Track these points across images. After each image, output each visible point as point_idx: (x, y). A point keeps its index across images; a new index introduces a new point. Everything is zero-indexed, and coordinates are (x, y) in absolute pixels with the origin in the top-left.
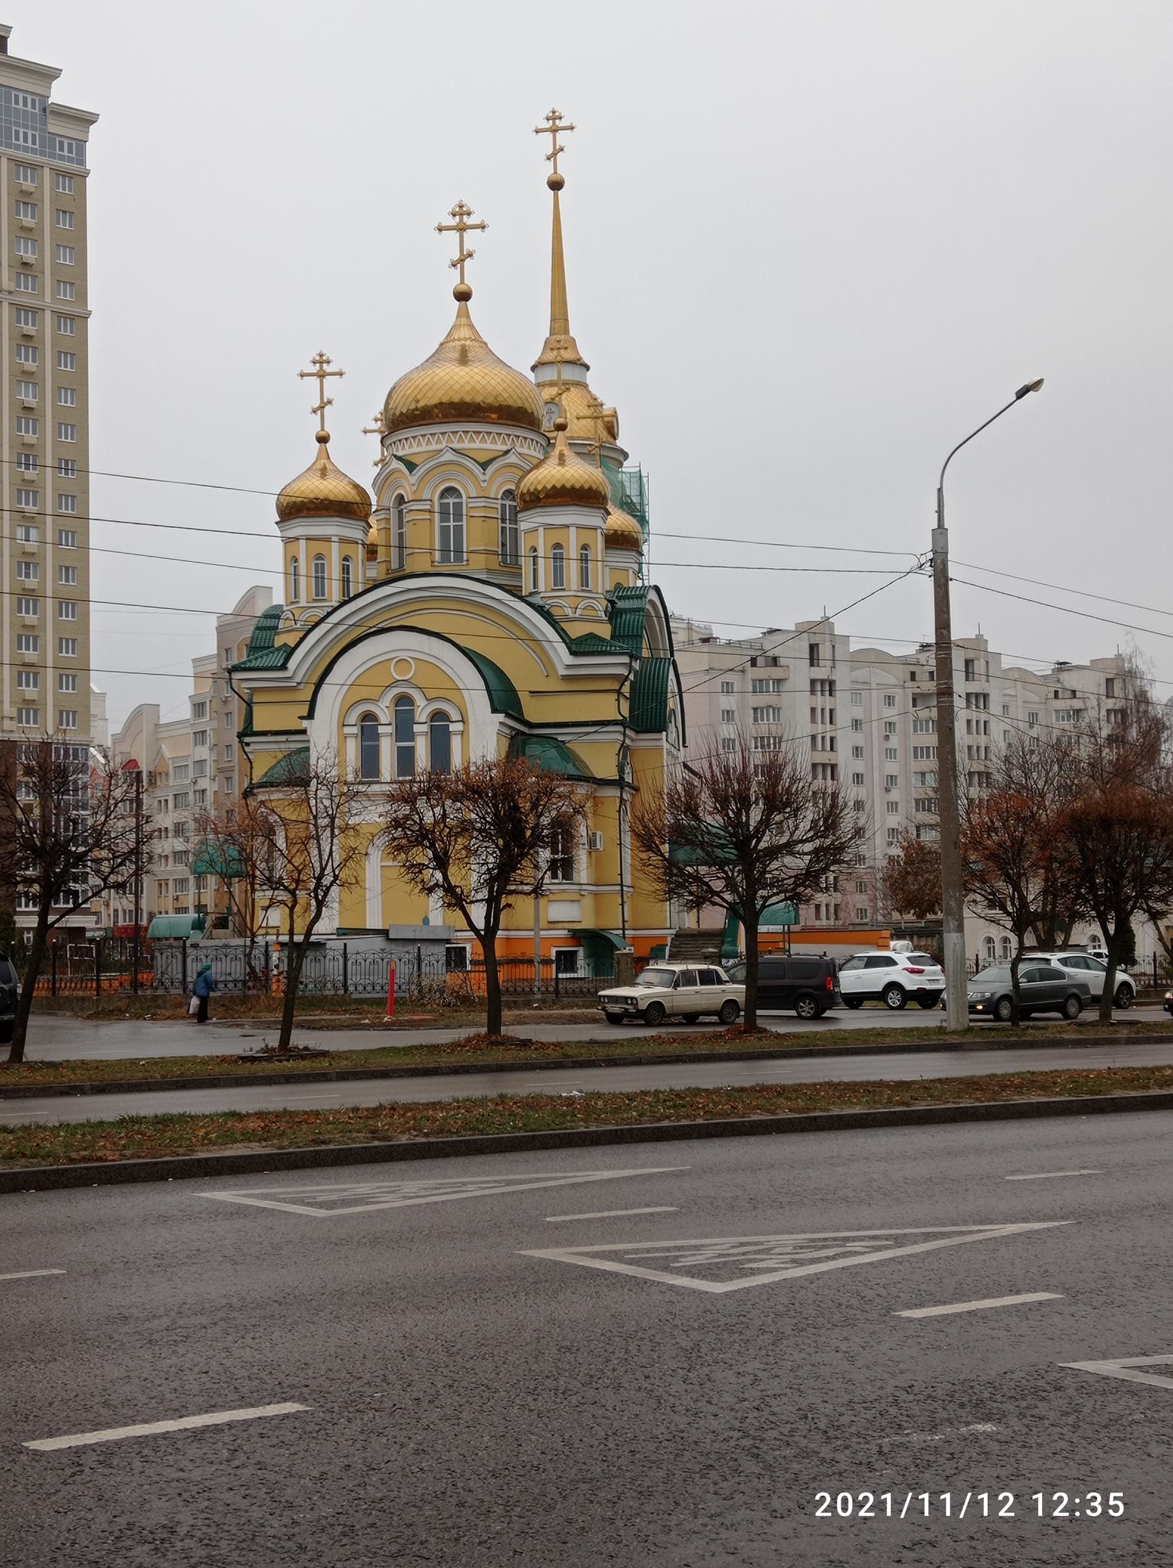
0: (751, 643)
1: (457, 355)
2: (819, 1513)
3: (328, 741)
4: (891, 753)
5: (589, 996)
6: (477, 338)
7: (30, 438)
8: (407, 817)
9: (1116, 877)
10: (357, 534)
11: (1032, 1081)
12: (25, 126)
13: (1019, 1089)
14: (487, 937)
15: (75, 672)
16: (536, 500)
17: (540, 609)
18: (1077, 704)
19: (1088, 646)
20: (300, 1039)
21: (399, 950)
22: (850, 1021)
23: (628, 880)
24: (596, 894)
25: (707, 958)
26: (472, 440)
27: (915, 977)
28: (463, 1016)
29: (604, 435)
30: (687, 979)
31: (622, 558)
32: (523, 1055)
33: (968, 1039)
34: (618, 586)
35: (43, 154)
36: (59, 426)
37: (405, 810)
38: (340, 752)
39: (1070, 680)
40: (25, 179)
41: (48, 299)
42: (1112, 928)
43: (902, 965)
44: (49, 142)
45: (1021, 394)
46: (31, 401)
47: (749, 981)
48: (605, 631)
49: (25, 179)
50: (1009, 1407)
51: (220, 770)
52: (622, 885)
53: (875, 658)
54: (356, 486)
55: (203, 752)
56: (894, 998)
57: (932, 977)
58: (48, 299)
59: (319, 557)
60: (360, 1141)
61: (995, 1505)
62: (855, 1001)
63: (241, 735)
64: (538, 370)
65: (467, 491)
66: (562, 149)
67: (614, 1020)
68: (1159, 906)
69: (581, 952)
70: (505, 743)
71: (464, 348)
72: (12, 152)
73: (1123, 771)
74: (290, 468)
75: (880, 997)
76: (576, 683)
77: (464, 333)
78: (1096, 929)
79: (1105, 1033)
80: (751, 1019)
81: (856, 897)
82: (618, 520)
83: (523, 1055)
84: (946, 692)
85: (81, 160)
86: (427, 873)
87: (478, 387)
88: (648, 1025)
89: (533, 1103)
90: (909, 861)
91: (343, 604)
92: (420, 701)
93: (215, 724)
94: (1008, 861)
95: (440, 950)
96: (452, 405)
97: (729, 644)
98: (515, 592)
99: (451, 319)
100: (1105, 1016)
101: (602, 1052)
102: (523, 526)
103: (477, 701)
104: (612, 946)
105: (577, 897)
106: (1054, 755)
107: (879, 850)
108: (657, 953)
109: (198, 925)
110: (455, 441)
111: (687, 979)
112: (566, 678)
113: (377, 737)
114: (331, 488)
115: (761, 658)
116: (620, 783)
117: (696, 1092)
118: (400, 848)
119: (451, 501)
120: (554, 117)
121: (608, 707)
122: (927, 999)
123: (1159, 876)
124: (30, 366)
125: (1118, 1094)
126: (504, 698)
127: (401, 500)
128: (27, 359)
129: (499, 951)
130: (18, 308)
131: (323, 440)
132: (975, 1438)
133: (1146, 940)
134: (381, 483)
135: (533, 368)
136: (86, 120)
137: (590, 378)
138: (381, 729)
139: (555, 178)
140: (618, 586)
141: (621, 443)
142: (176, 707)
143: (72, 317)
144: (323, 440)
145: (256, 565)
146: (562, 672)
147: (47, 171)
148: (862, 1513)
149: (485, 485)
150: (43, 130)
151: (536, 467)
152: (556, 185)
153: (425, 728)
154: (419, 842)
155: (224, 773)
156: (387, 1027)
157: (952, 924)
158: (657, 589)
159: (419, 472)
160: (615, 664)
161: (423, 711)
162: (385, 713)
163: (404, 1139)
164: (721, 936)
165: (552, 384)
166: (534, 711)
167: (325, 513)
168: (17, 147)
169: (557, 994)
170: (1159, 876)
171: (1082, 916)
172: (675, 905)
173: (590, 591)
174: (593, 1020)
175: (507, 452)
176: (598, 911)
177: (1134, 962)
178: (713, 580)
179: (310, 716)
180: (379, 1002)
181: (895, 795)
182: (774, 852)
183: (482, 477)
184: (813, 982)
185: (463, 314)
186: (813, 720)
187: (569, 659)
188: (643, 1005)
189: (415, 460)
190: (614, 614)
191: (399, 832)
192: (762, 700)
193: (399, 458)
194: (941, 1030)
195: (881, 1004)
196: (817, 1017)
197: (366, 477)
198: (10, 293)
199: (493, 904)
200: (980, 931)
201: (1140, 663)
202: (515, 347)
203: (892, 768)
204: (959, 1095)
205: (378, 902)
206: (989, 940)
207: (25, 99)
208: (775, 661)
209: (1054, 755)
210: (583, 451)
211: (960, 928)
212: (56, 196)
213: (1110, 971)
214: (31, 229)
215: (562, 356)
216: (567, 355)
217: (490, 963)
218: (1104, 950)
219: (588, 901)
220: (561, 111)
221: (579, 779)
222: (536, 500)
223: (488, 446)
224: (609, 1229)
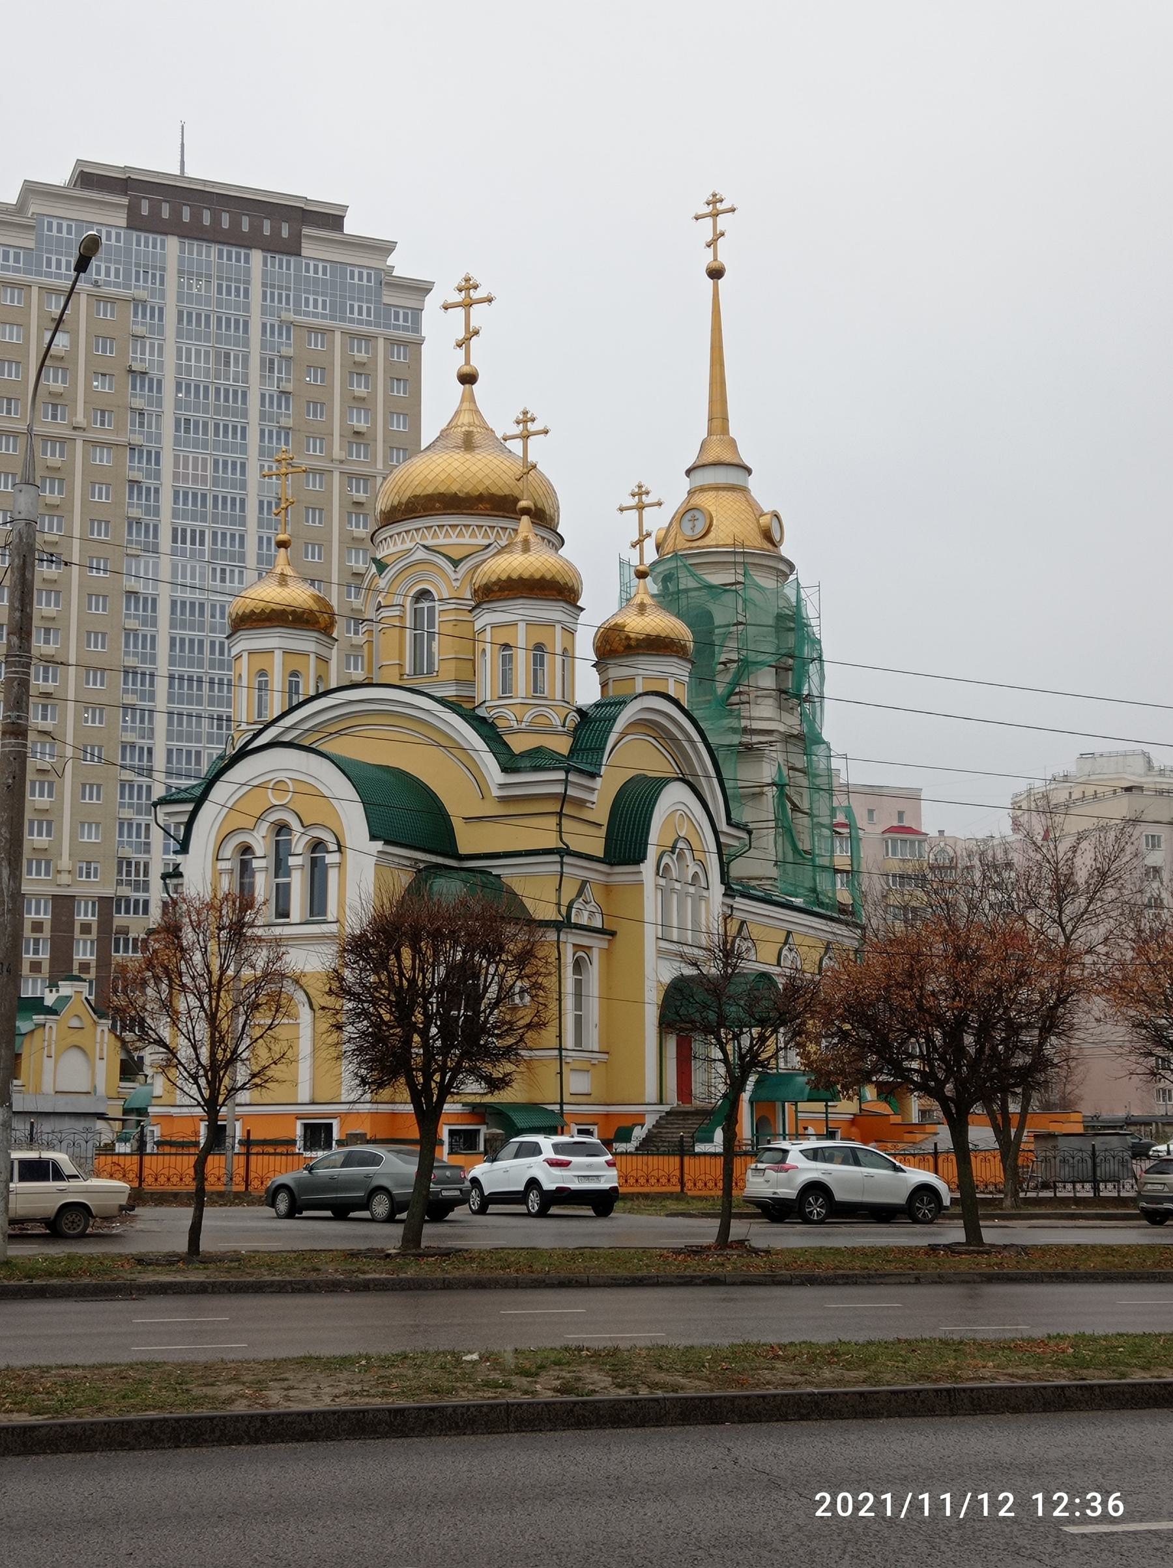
1: (460, 442)
2: (819, 1513)
12: (316, 293)
26: (447, 535)
27: (556, 1171)
35: (377, 325)
40: (359, 351)
41: (380, 466)
44: (384, 313)
49: (359, 351)
52: (560, 1049)
58: (380, 466)
59: (294, 674)
61: (995, 1505)
64: (692, 474)
65: (439, 592)
66: (722, 234)
72: (346, 325)
87: (455, 474)
105: (586, 1066)
110: (429, 538)
112: (503, 800)
119: (425, 605)
120: (715, 200)
128: (357, 526)
130: (350, 476)
137: (752, 482)
139: (715, 265)
141: (785, 551)
146: (496, 792)
147: (381, 342)
148: (862, 1513)
149: (457, 584)
150: (378, 302)
152: (716, 273)
159: (390, 573)
161: (299, 843)
162: (260, 841)
167: (268, 624)
168: (352, 321)
173: (545, 698)
175: (490, 545)
183: (453, 576)
185: (470, 398)
187: (501, 778)
189: (388, 561)
198: (341, 462)
207: (360, 274)
212: (389, 365)
214: (364, 399)
222: (494, 592)
223: (467, 540)
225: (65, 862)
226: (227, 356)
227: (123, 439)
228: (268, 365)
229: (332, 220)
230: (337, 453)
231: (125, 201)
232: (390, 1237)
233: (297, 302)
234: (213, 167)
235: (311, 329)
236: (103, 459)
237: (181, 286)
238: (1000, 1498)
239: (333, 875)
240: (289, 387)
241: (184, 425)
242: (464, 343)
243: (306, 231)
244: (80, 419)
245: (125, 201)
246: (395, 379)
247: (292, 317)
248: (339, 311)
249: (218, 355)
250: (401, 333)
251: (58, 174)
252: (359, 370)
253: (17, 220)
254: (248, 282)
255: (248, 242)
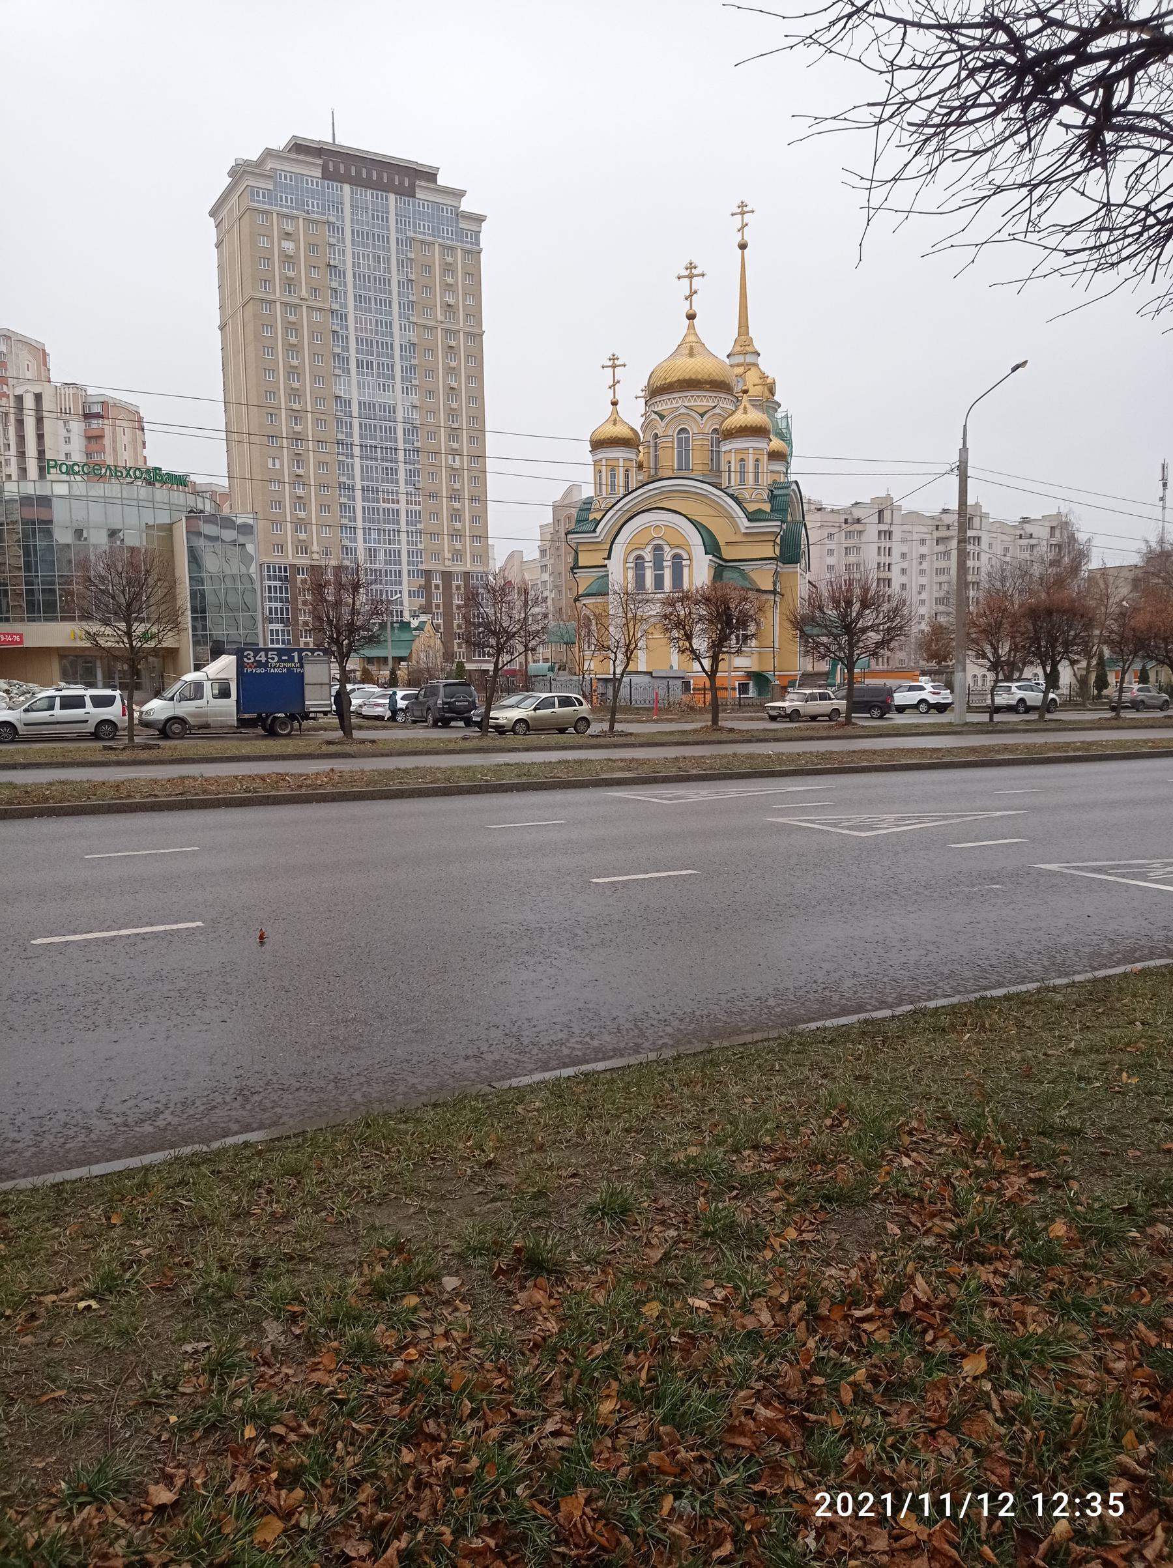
0: (845, 511)
3: (618, 572)
4: (922, 572)
5: (762, 707)
6: (699, 341)
7: (454, 405)
8: (671, 614)
9: (1053, 643)
10: (633, 456)
11: (1005, 748)
13: (998, 752)
14: (712, 675)
15: (481, 537)
16: (730, 434)
17: (731, 496)
18: (1033, 542)
19: (1039, 509)
20: (618, 727)
21: (657, 682)
22: (899, 719)
23: (777, 646)
24: (760, 653)
25: (820, 686)
28: (692, 716)
29: (767, 394)
30: (813, 697)
31: (779, 467)
32: (731, 736)
33: (965, 728)
34: (775, 481)
36: (469, 398)
37: (670, 610)
38: (626, 577)
39: (1029, 528)
42: (1048, 669)
43: (929, 690)
44: (460, 234)
45: (1014, 369)
46: (454, 384)
47: (849, 697)
48: (767, 507)
50: (1006, 880)
51: (555, 586)
53: (915, 517)
54: (632, 429)
55: (546, 577)
56: (923, 708)
57: (945, 696)
60: (674, 772)
62: (901, 709)
63: (572, 569)
67: (773, 719)
68: (1076, 657)
69: (751, 683)
70: (713, 571)
71: (691, 347)
73: (1060, 582)
74: (596, 420)
75: (915, 707)
76: (751, 537)
77: (692, 338)
78: (1039, 670)
79: (1042, 726)
80: (848, 718)
81: (902, 655)
82: (776, 444)
83: (731, 736)
84: (963, 541)
85: (478, 244)
86: (681, 642)
88: (791, 721)
89: (751, 756)
90: (934, 633)
91: (625, 496)
92: (667, 548)
93: (552, 561)
94: (991, 633)
95: (679, 682)
96: (685, 380)
97: (832, 511)
98: (717, 486)
99: (685, 331)
100: (1042, 716)
101: (771, 735)
102: (724, 449)
103: (698, 551)
104: (767, 680)
106: (1018, 572)
107: (919, 628)
108: (792, 684)
109: (551, 669)
111: (813, 697)
112: (745, 534)
113: (644, 568)
114: (620, 431)
115: (850, 521)
116: (774, 592)
117: (832, 753)
118: (667, 629)
121: (769, 551)
122: (941, 708)
123: (1078, 641)
124: (453, 364)
125: (1051, 755)
126: (712, 547)
127: (656, 436)
129: (718, 683)
131: (614, 404)
132: (992, 890)
133: (1066, 675)
134: (646, 426)
135: (728, 356)
136: (479, 219)
138: (646, 564)
140: (775, 481)
142: (532, 553)
143: (474, 335)
144: (614, 404)
145: (580, 475)
146: (744, 531)
151: (731, 415)
152: (743, 246)
153: (669, 563)
154: (678, 627)
155: (557, 588)
156: (655, 721)
157: (960, 668)
158: (796, 483)
159: (667, 420)
160: (773, 526)
161: (668, 553)
162: (648, 557)
163: (694, 772)
164: (826, 675)
165: (739, 365)
166: (727, 553)
168: (443, 238)
169: (740, 705)
170: (1078, 641)
171: (1032, 663)
172: (809, 660)
174: (762, 719)
176: (760, 661)
177: (1058, 688)
178: (825, 478)
179: (609, 558)
180: (648, 709)
181: (924, 596)
182: (864, 630)
184: (880, 699)
185: (691, 327)
186: (879, 554)
188: (789, 711)
190: (772, 498)
191: (667, 622)
192: (850, 543)
193: (656, 413)
194: (950, 724)
195: (915, 711)
196: (881, 717)
197: (637, 423)
199: (715, 661)
200: (974, 673)
201: (1072, 518)
202: (719, 342)
203: (923, 580)
204: (967, 754)
205: (660, 658)
206: (975, 676)
208: (858, 521)
209: (1018, 572)
210: (758, 404)
211: (964, 670)
212: (464, 265)
213: (1046, 693)
215: (744, 347)
216: (749, 349)
217: (714, 688)
218: (1042, 681)
219: (755, 656)
220: (746, 202)
221: (751, 590)
222: (730, 434)
224: (804, 811)
225: (315, 548)
226: (379, 257)
227: (327, 306)
228: (400, 263)
229: (430, 176)
230: (440, 317)
231: (321, 162)
232: (1111, 714)
233: (414, 227)
234: (352, 138)
235: (423, 242)
236: (317, 317)
237: (352, 214)
238: (1055, 1498)
239: (686, 571)
240: (413, 277)
241: (359, 298)
242: (689, 297)
243: (418, 183)
244: (304, 293)
245: (321, 162)
246: (467, 274)
247: (412, 234)
248: (436, 231)
249: (374, 257)
250: (427, 238)
251: (279, 143)
252: (448, 268)
253: (258, 171)
254: (388, 213)
255: (387, 188)
